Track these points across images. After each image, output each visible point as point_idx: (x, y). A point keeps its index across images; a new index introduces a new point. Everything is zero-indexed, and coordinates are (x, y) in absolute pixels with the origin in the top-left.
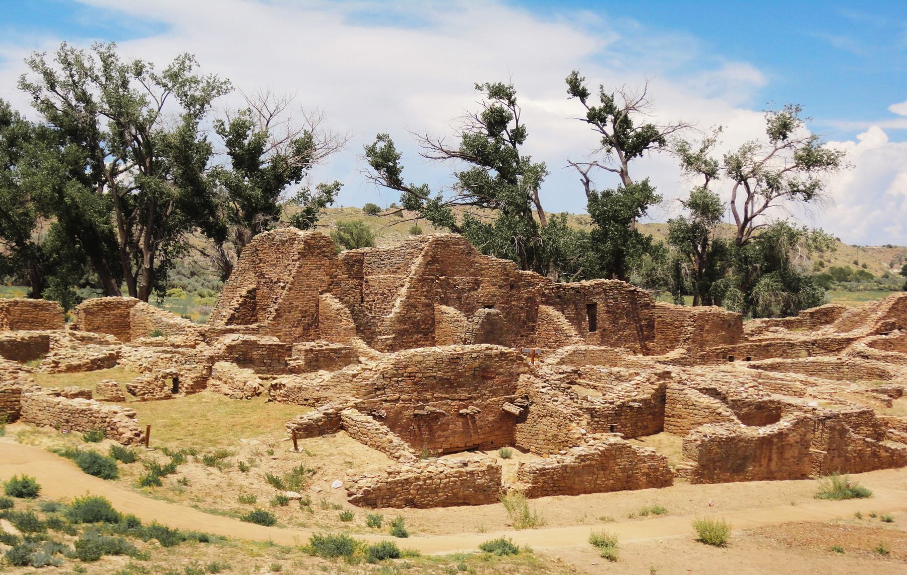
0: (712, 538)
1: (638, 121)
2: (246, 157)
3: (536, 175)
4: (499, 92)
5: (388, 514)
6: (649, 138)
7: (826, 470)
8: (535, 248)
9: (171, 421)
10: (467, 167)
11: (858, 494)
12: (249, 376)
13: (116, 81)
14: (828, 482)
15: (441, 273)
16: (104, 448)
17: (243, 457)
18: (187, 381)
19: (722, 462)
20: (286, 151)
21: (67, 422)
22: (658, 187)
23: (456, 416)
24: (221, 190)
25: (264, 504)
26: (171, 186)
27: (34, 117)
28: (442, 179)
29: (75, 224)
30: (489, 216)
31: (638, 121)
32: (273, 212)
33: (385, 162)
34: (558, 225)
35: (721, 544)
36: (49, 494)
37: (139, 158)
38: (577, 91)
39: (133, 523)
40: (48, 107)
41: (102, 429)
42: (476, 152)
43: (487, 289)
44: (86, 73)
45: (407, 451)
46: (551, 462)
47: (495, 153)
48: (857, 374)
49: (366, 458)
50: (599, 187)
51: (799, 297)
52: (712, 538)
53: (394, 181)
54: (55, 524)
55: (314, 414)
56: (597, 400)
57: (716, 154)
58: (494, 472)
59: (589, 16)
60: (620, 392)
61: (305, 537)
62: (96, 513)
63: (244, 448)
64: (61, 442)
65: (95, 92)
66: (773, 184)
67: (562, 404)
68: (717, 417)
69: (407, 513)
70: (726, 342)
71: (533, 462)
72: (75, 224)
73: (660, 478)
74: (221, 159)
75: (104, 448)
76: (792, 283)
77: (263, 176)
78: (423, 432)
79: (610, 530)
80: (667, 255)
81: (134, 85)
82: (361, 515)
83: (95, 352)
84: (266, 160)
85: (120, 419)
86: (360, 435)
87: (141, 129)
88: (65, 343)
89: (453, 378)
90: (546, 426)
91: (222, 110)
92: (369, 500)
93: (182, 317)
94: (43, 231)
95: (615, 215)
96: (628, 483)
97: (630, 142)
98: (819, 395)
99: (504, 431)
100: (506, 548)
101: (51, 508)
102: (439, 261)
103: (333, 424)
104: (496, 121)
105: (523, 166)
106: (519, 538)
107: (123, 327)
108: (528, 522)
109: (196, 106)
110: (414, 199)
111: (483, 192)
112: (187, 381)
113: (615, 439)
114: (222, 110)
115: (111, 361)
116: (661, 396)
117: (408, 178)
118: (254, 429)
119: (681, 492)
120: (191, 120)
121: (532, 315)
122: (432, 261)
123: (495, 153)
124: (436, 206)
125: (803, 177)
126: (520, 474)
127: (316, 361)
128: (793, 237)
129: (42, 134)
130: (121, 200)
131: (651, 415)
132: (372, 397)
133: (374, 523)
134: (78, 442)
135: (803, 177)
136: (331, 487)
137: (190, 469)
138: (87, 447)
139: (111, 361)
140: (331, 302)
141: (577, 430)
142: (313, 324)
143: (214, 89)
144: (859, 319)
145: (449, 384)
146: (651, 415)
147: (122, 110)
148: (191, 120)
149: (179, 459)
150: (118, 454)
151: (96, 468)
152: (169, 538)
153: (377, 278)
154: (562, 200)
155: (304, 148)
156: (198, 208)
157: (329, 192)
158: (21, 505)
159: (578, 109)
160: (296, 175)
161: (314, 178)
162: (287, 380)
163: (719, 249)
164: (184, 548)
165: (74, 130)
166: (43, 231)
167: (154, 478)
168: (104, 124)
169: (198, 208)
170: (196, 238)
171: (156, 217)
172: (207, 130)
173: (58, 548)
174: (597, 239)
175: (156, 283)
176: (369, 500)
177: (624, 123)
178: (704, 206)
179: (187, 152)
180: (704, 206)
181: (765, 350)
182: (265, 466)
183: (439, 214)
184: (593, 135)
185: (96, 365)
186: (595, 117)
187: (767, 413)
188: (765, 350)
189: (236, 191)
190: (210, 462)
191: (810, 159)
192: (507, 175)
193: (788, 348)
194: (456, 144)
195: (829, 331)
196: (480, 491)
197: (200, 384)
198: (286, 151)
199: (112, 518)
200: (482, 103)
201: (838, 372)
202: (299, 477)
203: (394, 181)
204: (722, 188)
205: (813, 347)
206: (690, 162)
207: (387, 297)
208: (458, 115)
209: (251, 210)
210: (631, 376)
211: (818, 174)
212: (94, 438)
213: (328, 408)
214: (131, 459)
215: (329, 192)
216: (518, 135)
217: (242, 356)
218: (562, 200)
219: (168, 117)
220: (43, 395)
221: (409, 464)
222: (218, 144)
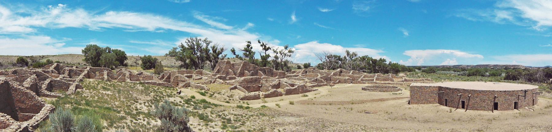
0: (292, 103)
1: (267, 46)
2: (215, 51)
3: (254, 53)
4: (249, 42)
5: (245, 101)
6: (269, 48)
7: (301, 93)
8: (254, 62)
9: (213, 87)
10: (244, 52)
11: (307, 96)
12: (221, 81)
13: (198, 42)
14: (303, 94)
15: (245, 66)
16: (203, 91)
17: (223, 93)
18: (213, 81)
19: (289, 92)
20: (220, 50)
21: (197, 87)
22: (271, 55)
23: (252, 86)
24: (211, 55)
25: (228, 100)
26: (204, 55)
27: (187, 46)
28: (241, 54)
29: (192, 60)
30: (248, 59)
31: (267, 46)
32: (218, 58)
33: (233, 51)
34: (257, 60)
35: (293, 104)
36: (197, 98)
37: (200, 52)
38: (259, 42)
39: (210, 103)
40: (188, 45)
41: (202, 88)
42: (246, 50)
43: (251, 68)
44: (194, 40)
45: (247, 92)
46: (267, 93)
47: (248, 50)
48: (300, 80)
49: (240, 93)
50: (262, 55)
51: (289, 69)
52: (292, 103)
53: (235, 54)
54: (199, 103)
55: (232, 87)
56: (271, 84)
57: (278, 51)
58: (259, 95)
59: (257, 33)
60: (274, 83)
61: (236, 105)
62: (204, 101)
63: (223, 91)
64: (197, 90)
65: (195, 43)
66: (285, 55)
67: (267, 84)
68: (287, 86)
69: (249, 101)
70: (283, 76)
71: (264, 93)
72: (192, 60)
73: (281, 95)
74: (211, 51)
75: (203, 91)
76: (288, 68)
77: (217, 53)
78: (248, 89)
79: (278, 103)
80: (177, 50)
81: (200, 42)
82: (242, 102)
83: (199, 77)
84: (217, 51)
85: (205, 87)
86: (239, 89)
87: (201, 47)
88: (194, 76)
89: (251, 81)
90: (265, 88)
91: (211, 45)
92: (242, 99)
93: (208, 73)
94: (188, 61)
95: (265, 58)
96: (277, 96)
97: (266, 49)
98: (299, 83)
99: (259, 89)
100: (264, 106)
101: (197, 100)
102: (245, 65)
103: (235, 88)
104: (248, 46)
105: (252, 52)
106: (266, 104)
107: (201, 74)
108: (265, 102)
109: (208, 44)
110: (237, 56)
111: (246, 56)
112: (213, 81)
113: (275, 90)
114: (211, 45)
115: (201, 78)
116: (279, 83)
117: (236, 54)
118: (224, 89)
119: (284, 97)
120: (207, 47)
121: (257, 72)
122: (244, 64)
123: (248, 50)
124: (240, 57)
125: (289, 54)
126: (262, 95)
127: (231, 79)
128: (288, 62)
129: (188, 48)
130: (198, 57)
131: (278, 86)
132: (241, 83)
133: (244, 103)
134: (199, 90)
135: (289, 54)
136: (236, 97)
137: (216, 95)
138: (201, 91)
139: (201, 78)
140: (230, 70)
141: (270, 88)
142: (228, 73)
143: (210, 42)
144: (299, 72)
145: (251, 82)
146: (278, 86)
147: (198, 45)
148: (207, 47)
149: (214, 93)
150: (205, 92)
151: (203, 94)
152: (216, 105)
153: (236, 67)
154: (257, 57)
155: (222, 50)
156: (208, 58)
157: (226, 56)
158: (193, 100)
159: (259, 45)
160: (221, 53)
161: (224, 54)
162: (228, 81)
163: (278, 63)
164: (218, 107)
165: (192, 48)
166: (188, 61)
167: (211, 96)
168: (196, 47)
169: (208, 58)
170: (208, 62)
171: (202, 59)
172: (209, 47)
173: (200, 107)
174: (262, 62)
175: (202, 67)
176: (242, 99)
177: (265, 46)
178: (276, 57)
179: (207, 51)
180: (276, 57)
181: (288, 77)
182: (227, 94)
183: (241, 58)
184: (261, 48)
185: (199, 79)
186: (261, 46)
187: (293, 85)
188: (288, 77)
189: (213, 56)
190: (218, 94)
191: (290, 52)
192: (250, 53)
193: (291, 76)
194: (243, 49)
195: (295, 74)
196: (257, 98)
197: (214, 82)
198: (220, 50)
199: (207, 102)
200: (247, 44)
201: (298, 79)
202: (231, 96)
203: (235, 54)
204: (279, 55)
205: (294, 76)
206: (275, 52)
207: (238, 69)
208: (244, 45)
209: (215, 58)
210: (275, 81)
211: (291, 54)
212: (201, 90)
213: (235, 85)
214: (207, 93)
215: (226, 56)
216: (251, 48)
217: (220, 78)
218: (257, 57)
219: (204, 46)
220: (193, 83)
221: (247, 94)
222: (211, 49)
